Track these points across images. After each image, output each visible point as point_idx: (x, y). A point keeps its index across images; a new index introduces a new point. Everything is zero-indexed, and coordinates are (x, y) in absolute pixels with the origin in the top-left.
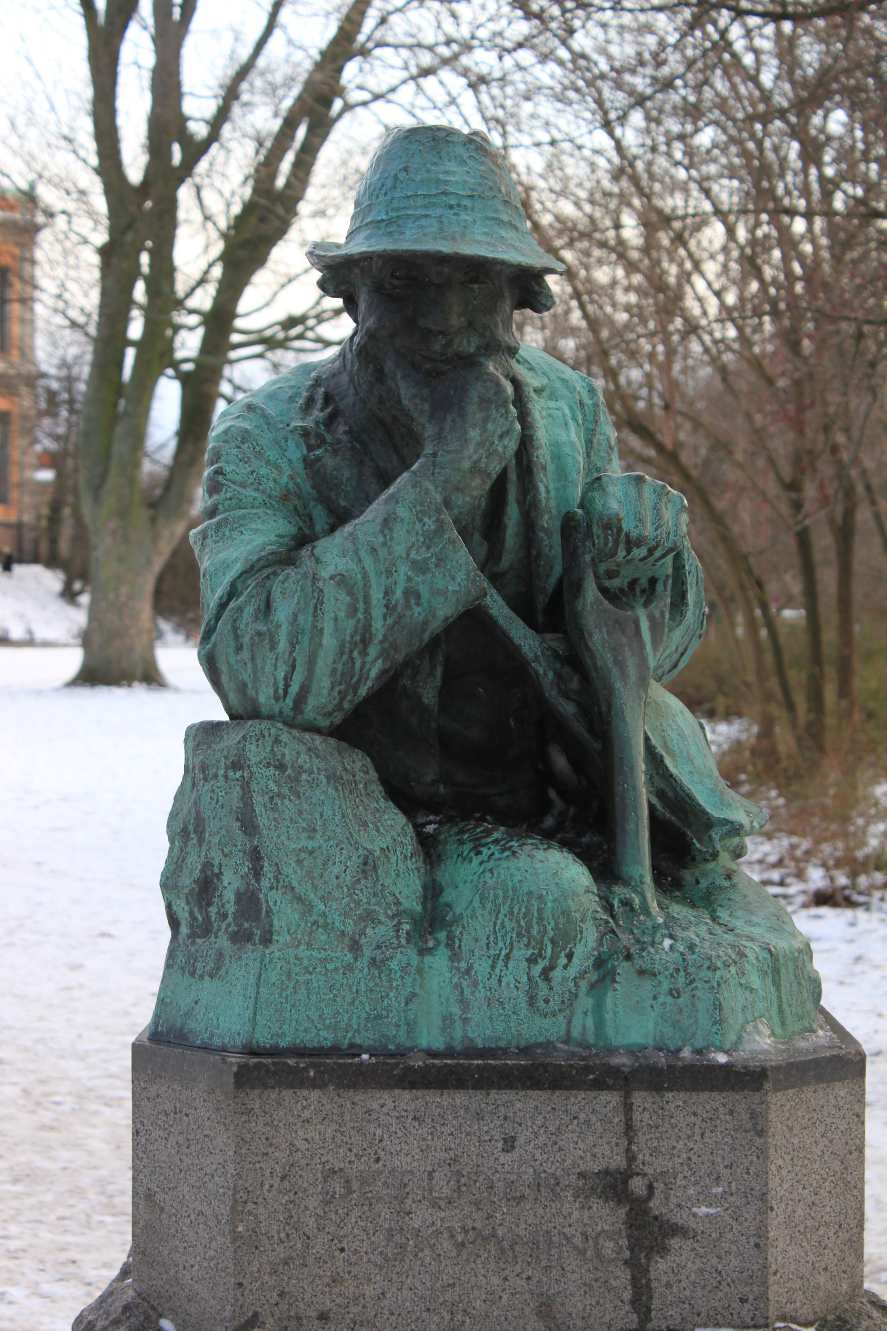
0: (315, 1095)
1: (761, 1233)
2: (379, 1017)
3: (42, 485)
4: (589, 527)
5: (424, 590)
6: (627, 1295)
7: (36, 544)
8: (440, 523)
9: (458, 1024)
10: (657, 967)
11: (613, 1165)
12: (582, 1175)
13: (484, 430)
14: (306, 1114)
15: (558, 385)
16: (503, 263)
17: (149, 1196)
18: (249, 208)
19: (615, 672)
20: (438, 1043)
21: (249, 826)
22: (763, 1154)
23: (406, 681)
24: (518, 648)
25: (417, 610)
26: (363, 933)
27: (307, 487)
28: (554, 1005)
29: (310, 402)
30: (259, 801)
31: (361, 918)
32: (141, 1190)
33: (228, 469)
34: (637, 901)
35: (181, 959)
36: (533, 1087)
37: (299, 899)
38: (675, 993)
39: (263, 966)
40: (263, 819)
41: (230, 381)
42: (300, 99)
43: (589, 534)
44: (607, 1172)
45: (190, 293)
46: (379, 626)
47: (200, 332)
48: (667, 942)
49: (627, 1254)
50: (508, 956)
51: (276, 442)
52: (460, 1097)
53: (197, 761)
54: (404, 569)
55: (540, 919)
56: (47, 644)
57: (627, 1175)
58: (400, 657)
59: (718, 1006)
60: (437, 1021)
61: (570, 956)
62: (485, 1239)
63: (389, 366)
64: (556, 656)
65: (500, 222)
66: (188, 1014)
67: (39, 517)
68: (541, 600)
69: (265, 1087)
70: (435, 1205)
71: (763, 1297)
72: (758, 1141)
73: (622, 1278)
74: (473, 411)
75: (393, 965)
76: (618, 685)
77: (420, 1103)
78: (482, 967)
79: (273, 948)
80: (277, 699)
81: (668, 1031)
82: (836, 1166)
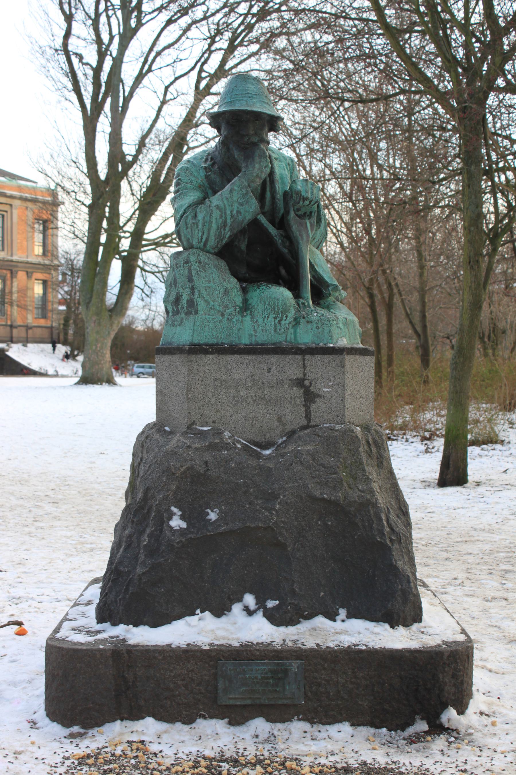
0: (211, 356)
1: (343, 396)
2: (230, 335)
3: (60, 312)
4: (292, 194)
5: (242, 211)
6: (304, 415)
7: (59, 334)
8: (247, 191)
9: (254, 337)
10: (312, 320)
11: (300, 377)
12: (290, 380)
13: (260, 165)
14: (209, 362)
15: (281, 158)
16: (265, 114)
17: (161, 392)
18: (149, 189)
19: (300, 238)
20: (248, 342)
21: (190, 279)
22: (344, 373)
23: (236, 243)
24: (270, 233)
25: (240, 217)
26: (225, 311)
27: (206, 184)
28: (282, 331)
29: (206, 160)
30: (194, 272)
31: (224, 307)
32: (159, 390)
33: (182, 178)
34: (306, 304)
35: (170, 322)
36: (276, 354)
37: (206, 301)
38: (318, 328)
39: (195, 320)
40: (195, 278)
41: (142, 259)
42: (170, 144)
43: (292, 197)
44: (298, 379)
45: (125, 225)
46: (229, 221)
47: (129, 240)
48: (315, 314)
49: (304, 403)
50: (268, 317)
51: (197, 171)
52: (254, 357)
53: (174, 263)
54: (236, 205)
55: (278, 306)
56: (63, 376)
57: (304, 380)
58: (235, 231)
59: (330, 332)
60: (247, 336)
61: (287, 317)
62: (262, 399)
63: (231, 146)
64: (282, 235)
65: (265, 103)
66: (173, 337)
67: (59, 324)
68: (277, 220)
69: (197, 354)
70: (247, 389)
71: (344, 415)
72: (342, 369)
73: (302, 410)
74: (257, 159)
75: (234, 320)
76: (301, 242)
77: (242, 359)
78: (260, 321)
79: (198, 315)
80: (198, 243)
81: (316, 339)
82: (366, 381)
